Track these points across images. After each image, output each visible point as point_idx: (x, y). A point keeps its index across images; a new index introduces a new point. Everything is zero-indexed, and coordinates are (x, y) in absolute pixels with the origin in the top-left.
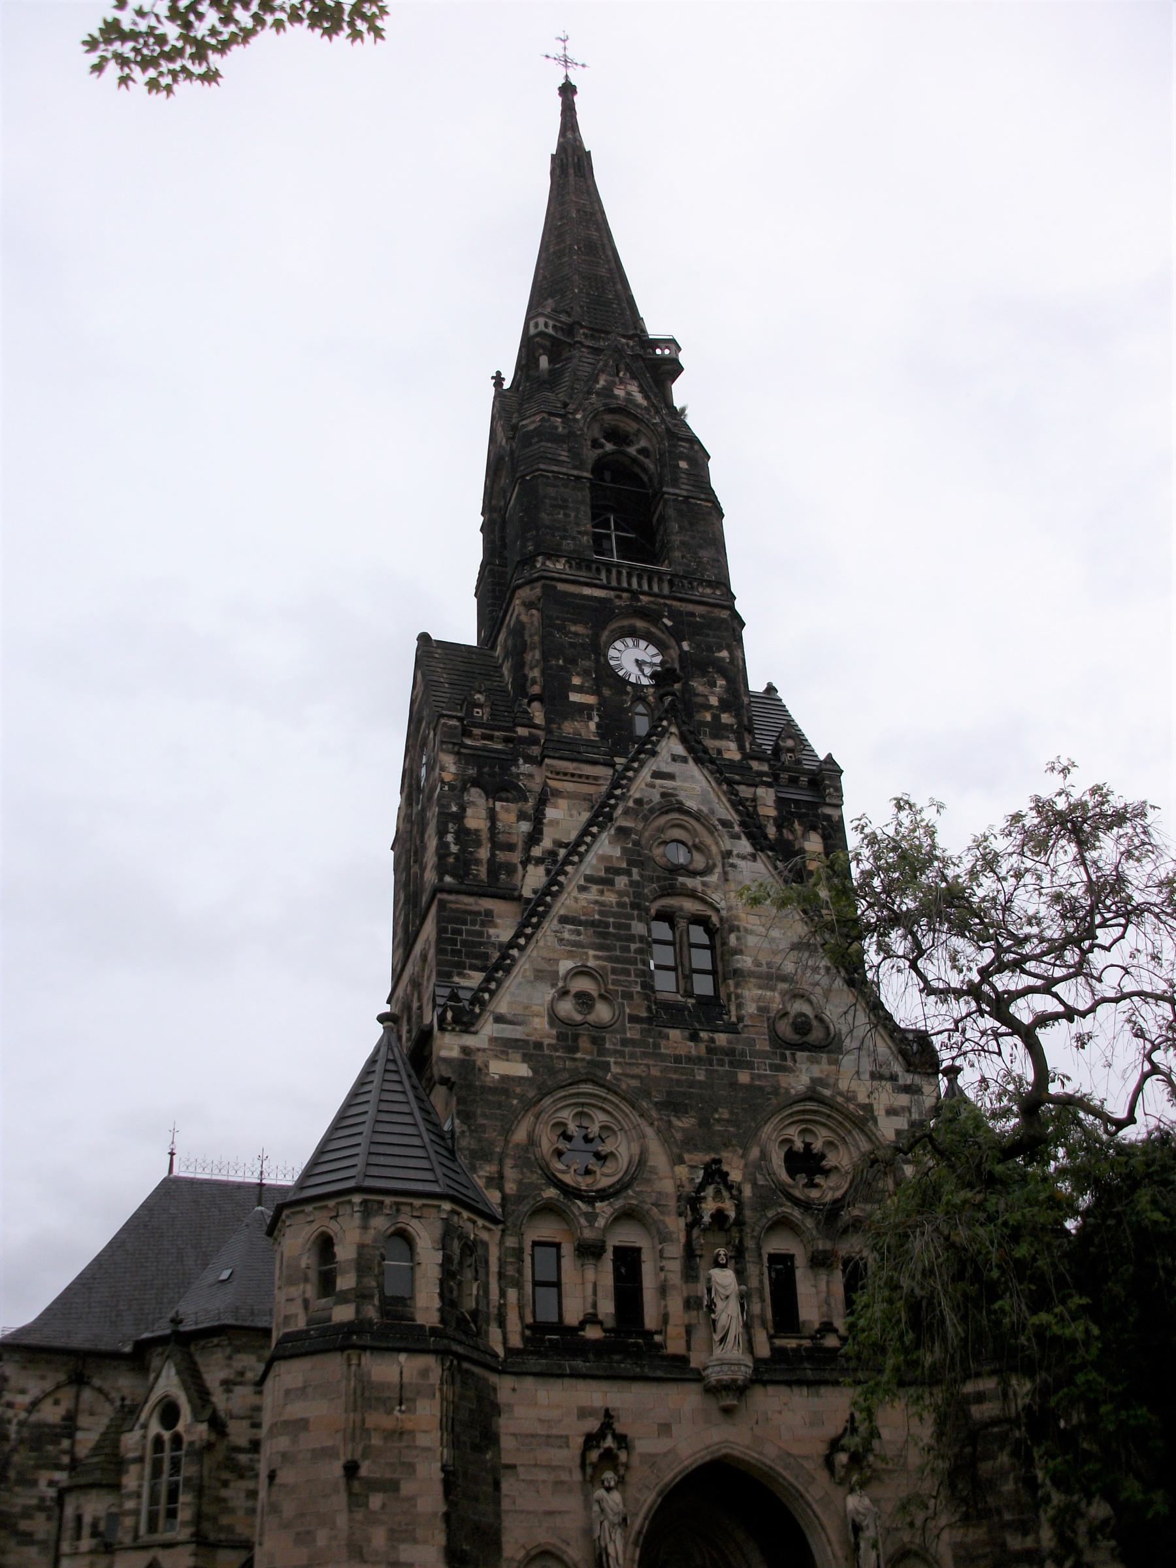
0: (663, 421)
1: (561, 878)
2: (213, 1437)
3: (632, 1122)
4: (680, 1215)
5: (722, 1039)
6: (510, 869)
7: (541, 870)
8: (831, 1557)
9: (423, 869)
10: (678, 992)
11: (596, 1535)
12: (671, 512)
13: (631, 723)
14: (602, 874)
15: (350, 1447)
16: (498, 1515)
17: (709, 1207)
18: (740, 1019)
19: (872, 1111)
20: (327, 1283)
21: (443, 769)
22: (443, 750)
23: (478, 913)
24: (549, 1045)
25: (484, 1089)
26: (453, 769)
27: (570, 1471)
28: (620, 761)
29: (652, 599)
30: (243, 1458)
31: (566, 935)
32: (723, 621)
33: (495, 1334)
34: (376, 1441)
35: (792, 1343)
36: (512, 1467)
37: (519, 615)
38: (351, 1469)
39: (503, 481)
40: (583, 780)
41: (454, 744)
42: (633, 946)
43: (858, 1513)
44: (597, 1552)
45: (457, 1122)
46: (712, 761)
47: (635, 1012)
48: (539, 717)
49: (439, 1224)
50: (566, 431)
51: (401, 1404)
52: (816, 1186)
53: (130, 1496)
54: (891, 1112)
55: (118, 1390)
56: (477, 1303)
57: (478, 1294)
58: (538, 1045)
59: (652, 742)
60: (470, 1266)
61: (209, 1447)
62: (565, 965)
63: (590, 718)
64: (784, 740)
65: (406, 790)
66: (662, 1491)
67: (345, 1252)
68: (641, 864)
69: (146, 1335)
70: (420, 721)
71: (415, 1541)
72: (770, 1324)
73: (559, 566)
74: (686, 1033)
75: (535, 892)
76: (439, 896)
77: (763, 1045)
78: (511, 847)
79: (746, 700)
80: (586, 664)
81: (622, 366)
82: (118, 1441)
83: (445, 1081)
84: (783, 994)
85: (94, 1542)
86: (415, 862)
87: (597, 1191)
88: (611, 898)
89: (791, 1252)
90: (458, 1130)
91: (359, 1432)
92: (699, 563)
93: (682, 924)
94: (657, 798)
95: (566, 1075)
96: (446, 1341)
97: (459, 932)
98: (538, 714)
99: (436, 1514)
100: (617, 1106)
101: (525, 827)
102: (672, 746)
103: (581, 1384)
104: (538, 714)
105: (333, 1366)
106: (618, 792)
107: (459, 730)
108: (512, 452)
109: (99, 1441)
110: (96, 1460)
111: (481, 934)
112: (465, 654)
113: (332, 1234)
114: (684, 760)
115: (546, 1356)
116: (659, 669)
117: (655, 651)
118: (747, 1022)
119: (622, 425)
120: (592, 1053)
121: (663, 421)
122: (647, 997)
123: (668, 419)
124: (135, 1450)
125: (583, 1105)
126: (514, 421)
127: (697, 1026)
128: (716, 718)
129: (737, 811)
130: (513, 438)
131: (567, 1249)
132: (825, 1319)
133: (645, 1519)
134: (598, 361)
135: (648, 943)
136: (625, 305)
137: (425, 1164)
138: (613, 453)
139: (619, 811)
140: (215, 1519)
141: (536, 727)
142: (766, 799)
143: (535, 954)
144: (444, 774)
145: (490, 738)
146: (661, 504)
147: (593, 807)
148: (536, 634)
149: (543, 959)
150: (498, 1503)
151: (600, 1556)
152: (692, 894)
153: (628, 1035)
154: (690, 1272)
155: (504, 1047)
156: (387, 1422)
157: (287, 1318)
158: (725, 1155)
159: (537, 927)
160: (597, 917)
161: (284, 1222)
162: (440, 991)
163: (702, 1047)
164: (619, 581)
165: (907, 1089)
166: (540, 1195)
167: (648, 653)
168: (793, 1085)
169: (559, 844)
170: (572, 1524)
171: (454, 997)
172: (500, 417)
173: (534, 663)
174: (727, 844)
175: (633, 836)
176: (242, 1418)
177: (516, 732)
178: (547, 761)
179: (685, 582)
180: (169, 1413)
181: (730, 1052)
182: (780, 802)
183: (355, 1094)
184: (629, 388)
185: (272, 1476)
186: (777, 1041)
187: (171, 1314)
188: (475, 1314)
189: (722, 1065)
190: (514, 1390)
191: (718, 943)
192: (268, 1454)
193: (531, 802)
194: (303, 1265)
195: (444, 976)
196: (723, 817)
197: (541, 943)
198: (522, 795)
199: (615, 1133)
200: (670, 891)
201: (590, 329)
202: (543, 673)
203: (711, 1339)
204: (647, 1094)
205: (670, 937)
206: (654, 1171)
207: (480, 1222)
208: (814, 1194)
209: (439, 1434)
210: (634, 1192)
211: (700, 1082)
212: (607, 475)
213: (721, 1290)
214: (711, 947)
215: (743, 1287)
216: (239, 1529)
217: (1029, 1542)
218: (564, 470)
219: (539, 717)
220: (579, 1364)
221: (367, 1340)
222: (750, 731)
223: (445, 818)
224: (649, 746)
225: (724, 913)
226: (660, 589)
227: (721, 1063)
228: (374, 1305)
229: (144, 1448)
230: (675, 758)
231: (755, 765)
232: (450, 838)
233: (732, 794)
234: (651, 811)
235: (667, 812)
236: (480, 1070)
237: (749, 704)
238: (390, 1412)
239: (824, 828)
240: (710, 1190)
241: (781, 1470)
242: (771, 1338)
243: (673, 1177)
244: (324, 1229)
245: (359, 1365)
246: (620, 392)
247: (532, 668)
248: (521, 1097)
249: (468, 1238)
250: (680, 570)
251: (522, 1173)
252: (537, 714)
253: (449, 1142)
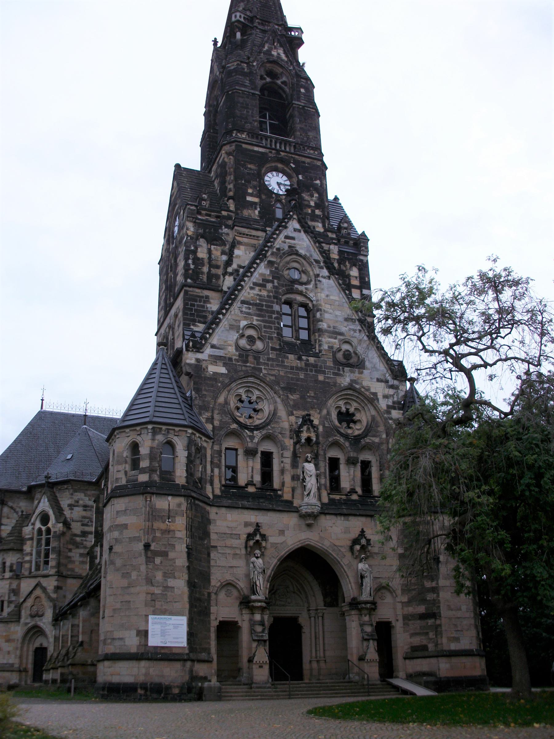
0: (294, 68)
1: (242, 283)
2: (65, 530)
3: (271, 395)
4: (291, 438)
5: (312, 360)
6: (217, 277)
7: (232, 278)
8: (350, 589)
9: (176, 275)
10: (292, 337)
11: (251, 577)
12: (296, 113)
13: (274, 212)
14: (261, 282)
15: (146, 536)
16: (209, 567)
17: (304, 435)
18: (320, 351)
19: (377, 396)
20: (135, 464)
21: (187, 229)
22: (188, 220)
23: (203, 297)
24: (235, 359)
25: (206, 378)
26: (192, 229)
27: (241, 550)
29: (286, 154)
30: (78, 539)
31: (244, 309)
32: (318, 166)
33: (209, 488)
34: (158, 534)
35: (337, 497)
36: (215, 547)
37: (224, 158)
38: (147, 546)
39: (216, 92)
40: (248, 237)
41: (193, 218)
42: (274, 316)
43: (363, 571)
44: (252, 584)
45: (193, 393)
46: (312, 233)
47: (274, 346)
48: (232, 207)
49: (186, 439)
50: (249, 71)
51: (169, 519)
52: (350, 428)
53: (27, 554)
54: (386, 397)
55: (20, 507)
56: (201, 475)
57: (202, 471)
58: (230, 359)
59: (285, 222)
60: (199, 458)
61: (63, 534)
62: (243, 323)
63: (256, 209)
64: (343, 223)
65: (167, 237)
66: (280, 559)
67: (144, 450)
68: (278, 278)
69: (32, 484)
70: (175, 205)
71: (175, 578)
72: (328, 488)
73: (244, 136)
74: (296, 357)
75: (229, 288)
76: (185, 288)
77: (330, 364)
78: (218, 267)
79: (327, 204)
80: (255, 183)
81: (276, 40)
82: (22, 530)
83: (188, 374)
84: (340, 340)
85: (11, 574)
86: (171, 271)
87: (255, 426)
89: (338, 457)
90: (194, 396)
91: (150, 530)
92: (308, 138)
93: (296, 306)
94: (286, 248)
96: (189, 491)
97: (193, 305)
98: (232, 205)
99: (184, 566)
100: (264, 388)
101: (225, 258)
102: (294, 224)
103: (246, 512)
104: (232, 205)
105: (139, 501)
106: (269, 244)
107: (196, 212)
108: (222, 79)
109: (11, 530)
110: (11, 538)
111: (203, 307)
112: (197, 175)
113: (138, 442)
114: (299, 231)
115: (230, 499)
116: (289, 188)
117: (286, 179)
118: (323, 353)
119: (274, 69)
120: (253, 364)
121: (294, 68)
122: (279, 340)
123: (296, 68)
124: (29, 534)
125: (249, 387)
126: (223, 64)
127: (301, 354)
128: (313, 212)
129: (323, 256)
130: (223, 72)
131: (241, 452)
132: (352, 487)
133: (272, 570)
134: (265, 37)
135: (281, 314)
136: (278, 8)
137: (179, 411)
138: (270, 83)
139: (269, 253)
140: (66, 565)
141: (231, 211)
142: (334, 250)
143: (230, 317)
144: (188, 232)
146: (291, 109)
147: (256, 250)
148: (232, 168)
149: (234, 320)
150: (209, 562)
151: (253, 586)
152: (301, 293)
153: (271, 356)
154: (295, 464)
155: (215, 359)
156: (163, 526)
157: (117, 479)
158: (311, 412)
159: (231, 305)
160: (258, 302)
161: (115, 436)
162: (186, 333)
163: (303, 363)
164: (271, 145)
165: (392, 387)
166: (229, 427)
167: (282, 179)
168: (343, 382)
169: (240, 267)
170: (241, 572)
171: (193, 336)
172: (216, 61)
173: (230, 181)
174: (317, 271)
175: (275, 265)
176: (78, 521)
177: (221, 213)
178: (236, 228)
179: (301, 147)
180: (45, 519)
181: (315, 366)
182: (340, 252)
183: (147, 378)
184: (279, 51)
185: (111, 549)
186: (336, 362)
187: (46, 474)
188: (200, 479)
189: (312, 372)
190: (217, 513)
191: (311, 316)
192: (108, 539)
193: (227, 247)
194: (125, 456)
195: (186, 325)
196: (316, 259)
197: (233, 313)
198: (223, 243)
199: (263, 400)
200: (291, 291)
201: (260, 20)
202: (235, 186)
203: (303, 494)
204: (278, 384)
205: (290, 313)
206: (280, 418)
207: (204, 438)
208: (350, 431)
209: (185, 532)
210: (271, 427)
211: (302, 379)
212: (266, 93)
213: (308, 472)
214: (308, 318)
215: (318, 472)
216: (77, 570)
217: (434, 584)
218: (247, 90)
219: (232, 207)
220: (245, 503)
221: (154, 490)
222: (328, 218)
223: (188, 253)
224: (284, 224)
225: (314, 302)
226: (290, 149)
227: (311, 371)
228: (157, 475)
229: (33, 533)
230: (295, 230)
231: (330, 234)
232: (190, 261)
233: (320, 248)
234: (284, 254)
235: (291, 255)
236: (204, 369)
237: (328, 206)
238: (164, 522)
239: (359, 266)
240: (305, 428)
241: (331, 552)
242: (329, 494)
243: (289, 421)
244: (134, 439)
245: (150, 501)
246: (274, 53)
247: (229, 184)
248: (222, 383)
249: (198, 445)
250: (299, 141)
251: (222, 417)
252: (231, 205)
253: (190, 401)
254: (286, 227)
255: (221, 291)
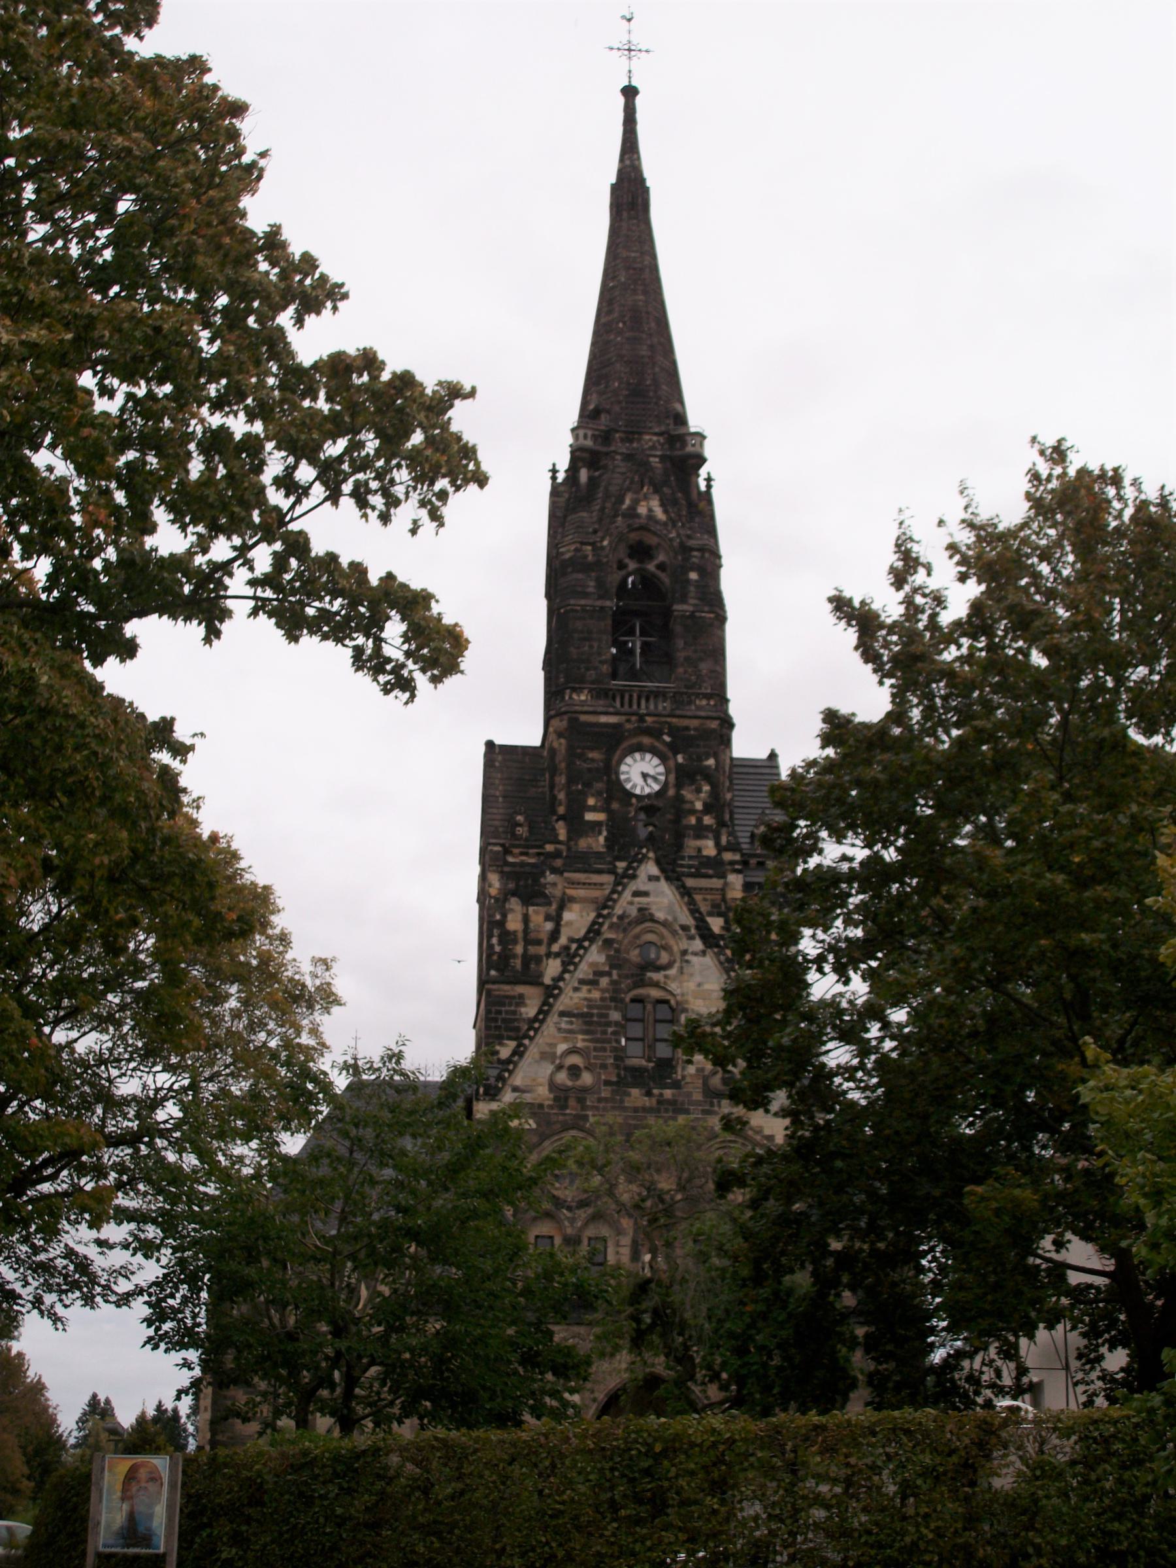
1: (561, 984)
5: (668, 1093)
6: (538, 959)
18: (684, 1077)
23: (513, 997)
28: (621, 865)
31: (563, 1026)
42: (610, 1030)
48: (562, 834)
58: (541, 1106)
62: (562, 1047)
63: (600, 833)
77: (698, 1096)
78: (538, 942)
88: (596, 995)
95: (559, 1126)
98: (562, 833)
101: (549, 926)
106: (605, 912)
111: (514, 1013)
114: (657, 879)
122: (617, 1067)
128: (699, 820)
129: (695, 918)
139: (606, 927)
141: (560, 842)
145: (526, 854)
152: (656, 985)
163: (654, 1100)
169: (572, 940)
193: (554, 906)
200: (641, 982)
202: (567, 795)
218: (589, 602)
219: (562, 834)
230: (652, 878)
232: (495, 941)
234: (630, 924)
246: (642, 510)
254: (634, 877)
255: (542, 984)
